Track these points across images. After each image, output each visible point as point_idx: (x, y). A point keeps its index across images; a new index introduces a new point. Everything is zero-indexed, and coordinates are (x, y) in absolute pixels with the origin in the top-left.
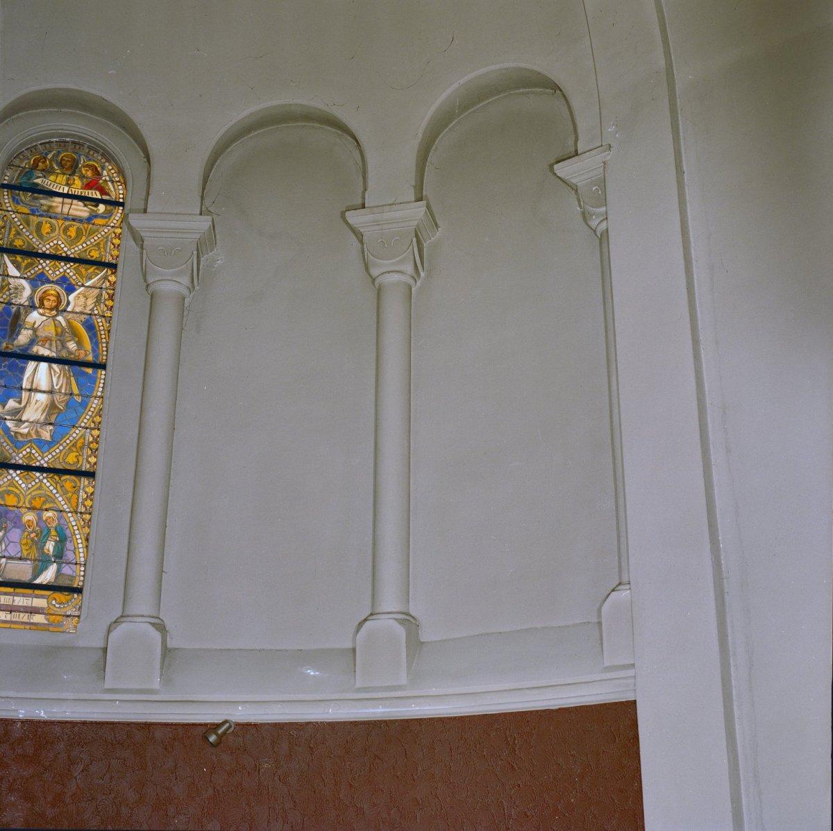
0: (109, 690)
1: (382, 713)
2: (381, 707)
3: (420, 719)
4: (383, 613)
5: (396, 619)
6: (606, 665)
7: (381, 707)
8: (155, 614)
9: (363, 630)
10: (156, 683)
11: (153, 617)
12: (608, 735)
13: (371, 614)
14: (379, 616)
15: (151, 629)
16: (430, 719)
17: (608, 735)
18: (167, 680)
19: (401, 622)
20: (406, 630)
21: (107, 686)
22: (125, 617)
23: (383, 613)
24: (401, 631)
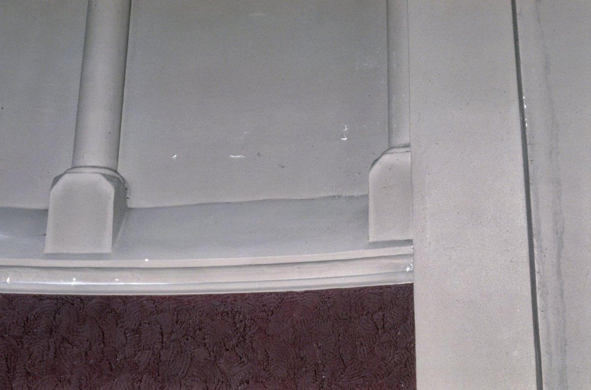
0: (50, 254)
1: (75, 286)
2: (74, 279)
3: (125, 297)
4: (86, 167)
5: (104, 175)
6: (371, 240)
7: (74, 279)
8: (114, 168)
9: (61, 182)
10: (107, 246)
11: (100, 168)
12: (378, 322)
13: (72, 168)
14: (83, 170)
15: (104, 181)
16: (137, 297)
17: (378, 322)
18: (121, 244)
19: (109, 178)
20: (115, 188)
21: (49, 248)
22: (75, 167)
23: (86, 167)
24: (109, 189)
